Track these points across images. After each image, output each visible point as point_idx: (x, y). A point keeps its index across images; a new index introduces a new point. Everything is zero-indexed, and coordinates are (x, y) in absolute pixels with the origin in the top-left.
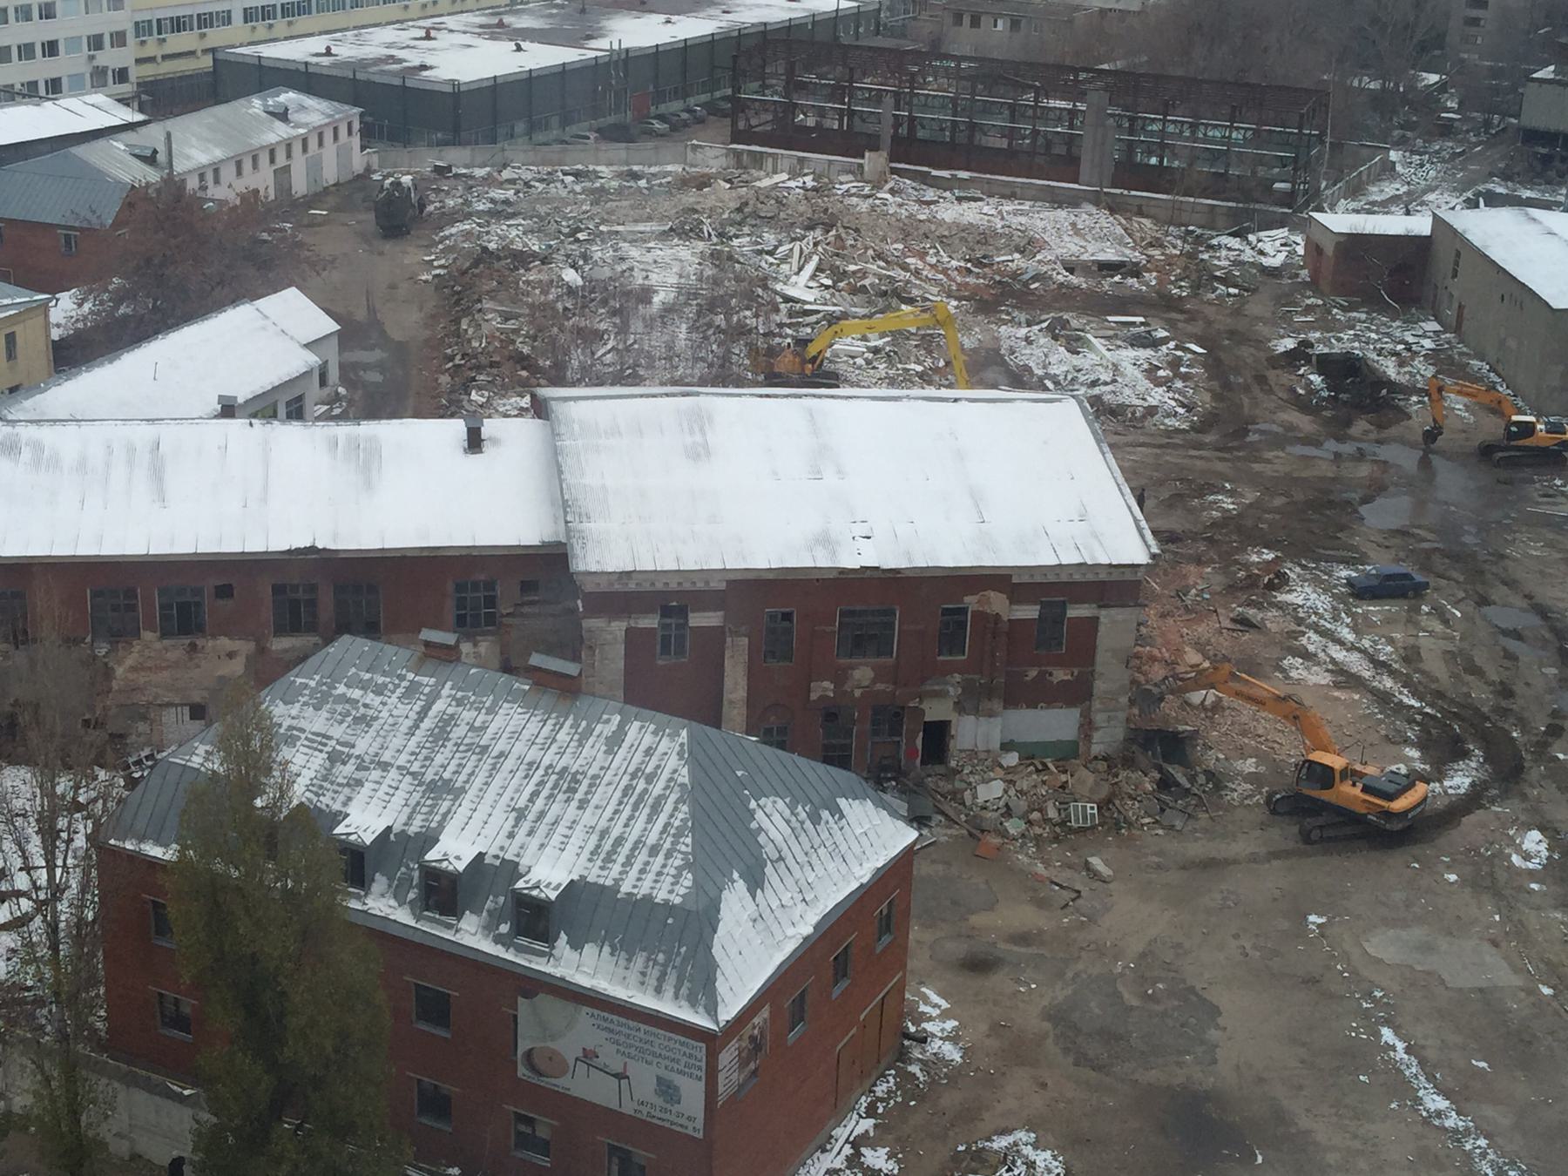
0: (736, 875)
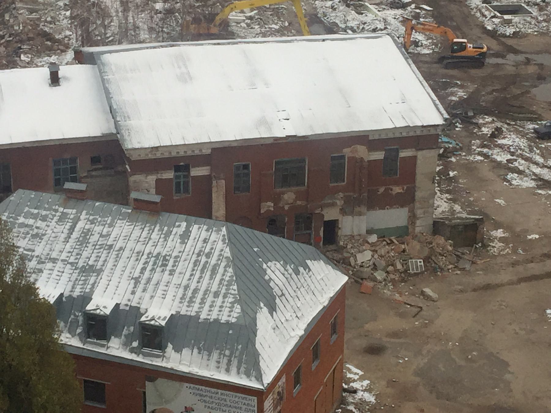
0: (262, 305)
